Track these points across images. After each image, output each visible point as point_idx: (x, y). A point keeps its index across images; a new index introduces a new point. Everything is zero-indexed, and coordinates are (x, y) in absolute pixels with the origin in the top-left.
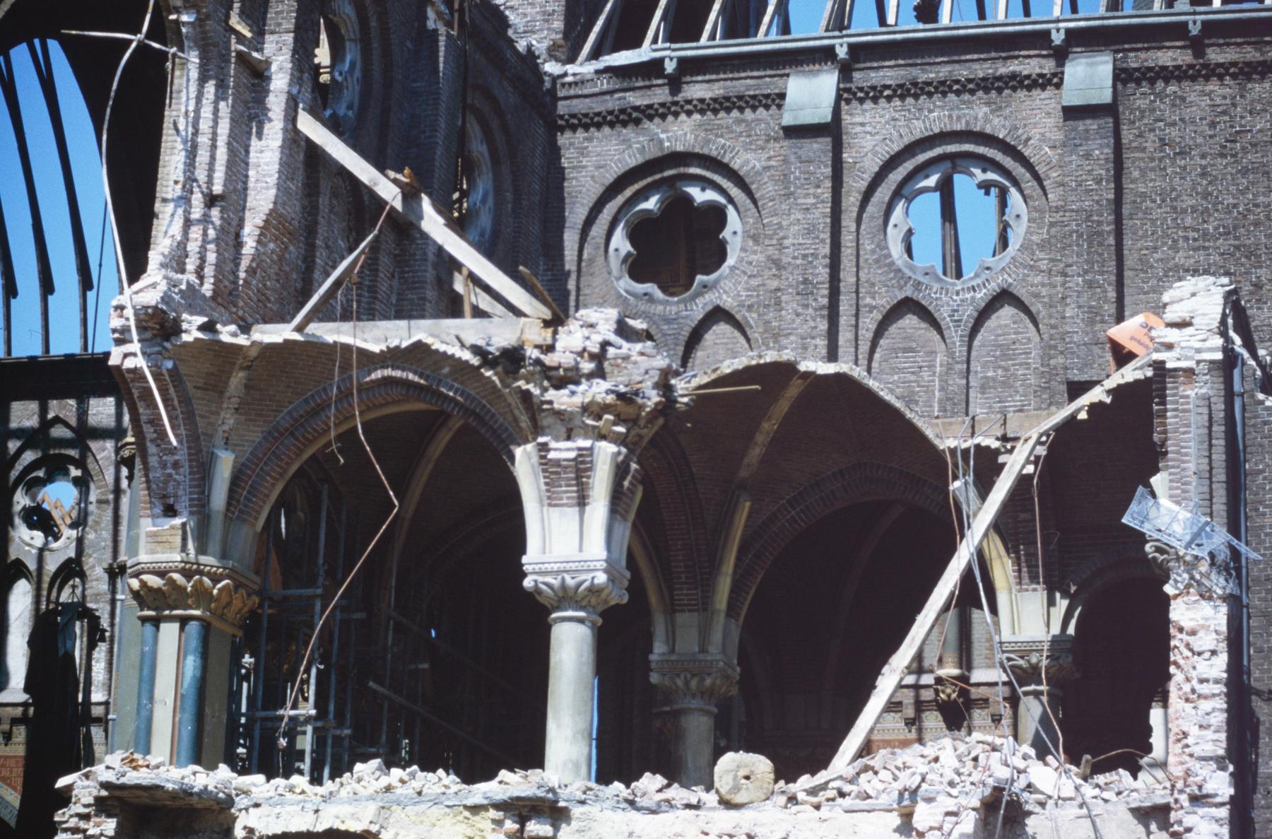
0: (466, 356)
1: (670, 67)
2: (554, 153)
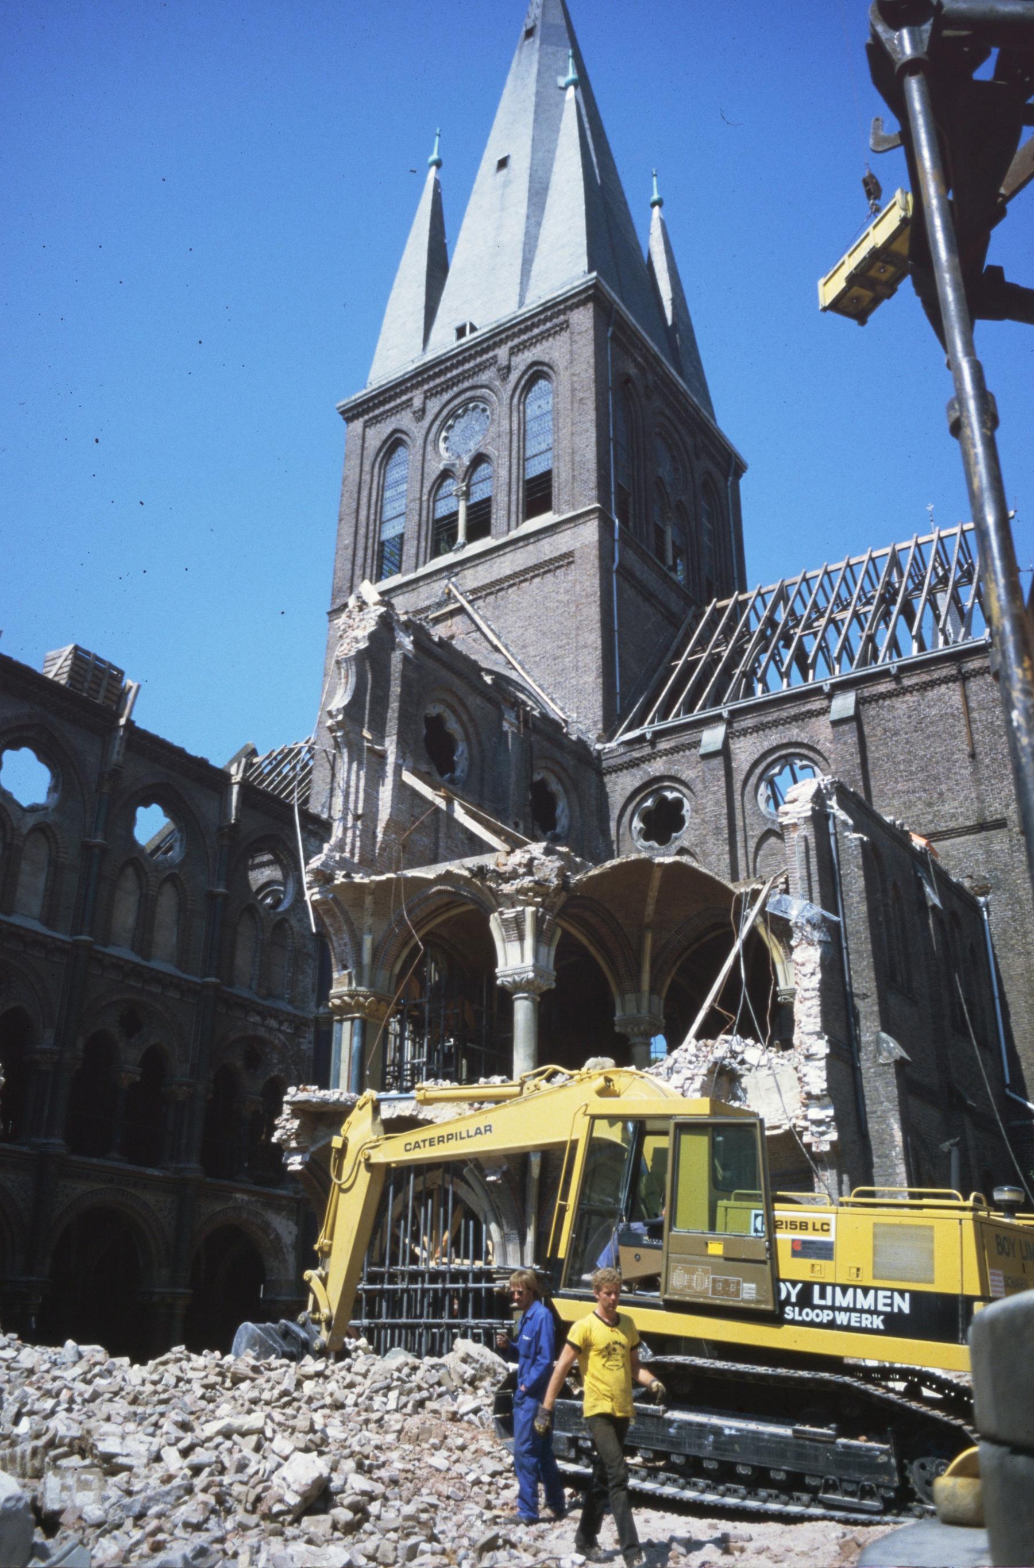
0: (466, 873)
1: (649, 736)
2: (602, 786)
